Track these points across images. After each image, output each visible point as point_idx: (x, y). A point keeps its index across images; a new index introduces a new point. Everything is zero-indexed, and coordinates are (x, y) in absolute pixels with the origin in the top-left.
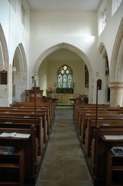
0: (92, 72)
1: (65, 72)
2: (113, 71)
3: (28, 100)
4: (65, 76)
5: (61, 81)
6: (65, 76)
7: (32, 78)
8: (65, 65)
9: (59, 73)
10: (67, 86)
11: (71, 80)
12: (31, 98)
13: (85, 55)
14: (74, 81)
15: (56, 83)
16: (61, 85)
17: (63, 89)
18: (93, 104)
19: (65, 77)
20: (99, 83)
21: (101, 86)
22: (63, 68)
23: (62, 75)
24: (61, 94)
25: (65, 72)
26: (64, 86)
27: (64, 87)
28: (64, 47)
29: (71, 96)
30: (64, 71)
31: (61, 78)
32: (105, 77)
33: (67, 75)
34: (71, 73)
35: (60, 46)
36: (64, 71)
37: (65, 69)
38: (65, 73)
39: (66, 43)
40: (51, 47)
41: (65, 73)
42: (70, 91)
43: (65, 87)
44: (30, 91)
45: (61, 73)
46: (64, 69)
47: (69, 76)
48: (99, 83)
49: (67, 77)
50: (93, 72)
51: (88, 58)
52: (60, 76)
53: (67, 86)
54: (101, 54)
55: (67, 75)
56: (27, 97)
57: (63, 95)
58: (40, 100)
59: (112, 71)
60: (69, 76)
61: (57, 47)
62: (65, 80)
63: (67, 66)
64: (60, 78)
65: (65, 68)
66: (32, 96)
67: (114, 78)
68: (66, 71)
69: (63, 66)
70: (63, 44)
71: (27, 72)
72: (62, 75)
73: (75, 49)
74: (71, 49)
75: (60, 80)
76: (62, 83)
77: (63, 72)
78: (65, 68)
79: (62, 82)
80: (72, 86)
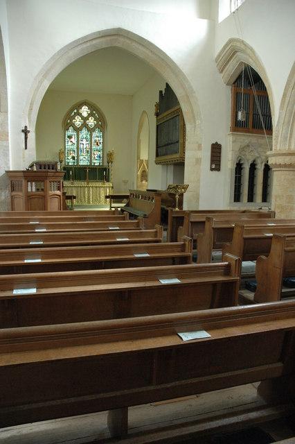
0: (195, 122)
1: (85, 122)
2: (289, 122)
3: (20, 203)
4: (84, 133)
5: (75, 146)
6: (84, 133)
7: (23, 135)
8: (84, 103)
9: (68, 124)
10: (91, 161)
11: (101, 146)
12: (29, 197)
13: (180, 71)
14: (109, 149)
15: (62, 153)
16: (73, 158)
17: (84, 168)
18: (201, 208)
19: (85, 136)
20: (216, 150)
21: (220, 161)
22: (78, 111)
23: (78, 130)
24: (77, 183)
25: (85, 122)
26: (84, 162)
27: (81, 163)
28: (120, 43)
29: (105, 189)
30: (83, 118)
31: (72, 140)
32: (231, 138)
33: (91, 130)
34: (102, 125)
35: (108, 38)
36: (83, 118)
37: (85, 114)
38: (85, 125)
39: (129, 32)
40: (83, 38)
41: (85, 125)
42: (99, 174)
43: (85, 164)
44: (29, 175)
45: (73, 125)
46: (80, 115)
47: (96, 133)
48: (216, 150)
49: (91, 135)
50: (198, 122)
51: (187, 81)
52: (70, 132)
53: (91, 161)
54: (222, 75)
55: (91, 130)
56: (14, 193)
57: (83, 184)
58: (56, 201)
59: (286, 120)
60: (96, 133)
61: (97, 41)
62: (85, 144)
63: (92, 107)
64: (70, 137)
65: (85, 111)
66: (29, 190)
67: (291, 137)
68: (87, 119)
69: (80, 106)
70: (118, 33)
71: (7, 112)
72: (78, 130)
73: (150, 54)
74: (140, 51)
75: (70, 143)
76: (78, 153)
77: (78, 121)
78: (85, 111)
79: (78, 148)
80: (106, 160)
